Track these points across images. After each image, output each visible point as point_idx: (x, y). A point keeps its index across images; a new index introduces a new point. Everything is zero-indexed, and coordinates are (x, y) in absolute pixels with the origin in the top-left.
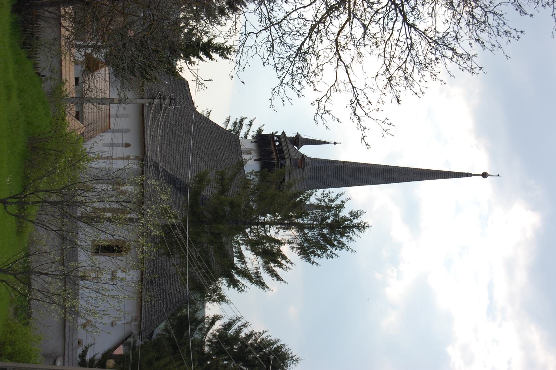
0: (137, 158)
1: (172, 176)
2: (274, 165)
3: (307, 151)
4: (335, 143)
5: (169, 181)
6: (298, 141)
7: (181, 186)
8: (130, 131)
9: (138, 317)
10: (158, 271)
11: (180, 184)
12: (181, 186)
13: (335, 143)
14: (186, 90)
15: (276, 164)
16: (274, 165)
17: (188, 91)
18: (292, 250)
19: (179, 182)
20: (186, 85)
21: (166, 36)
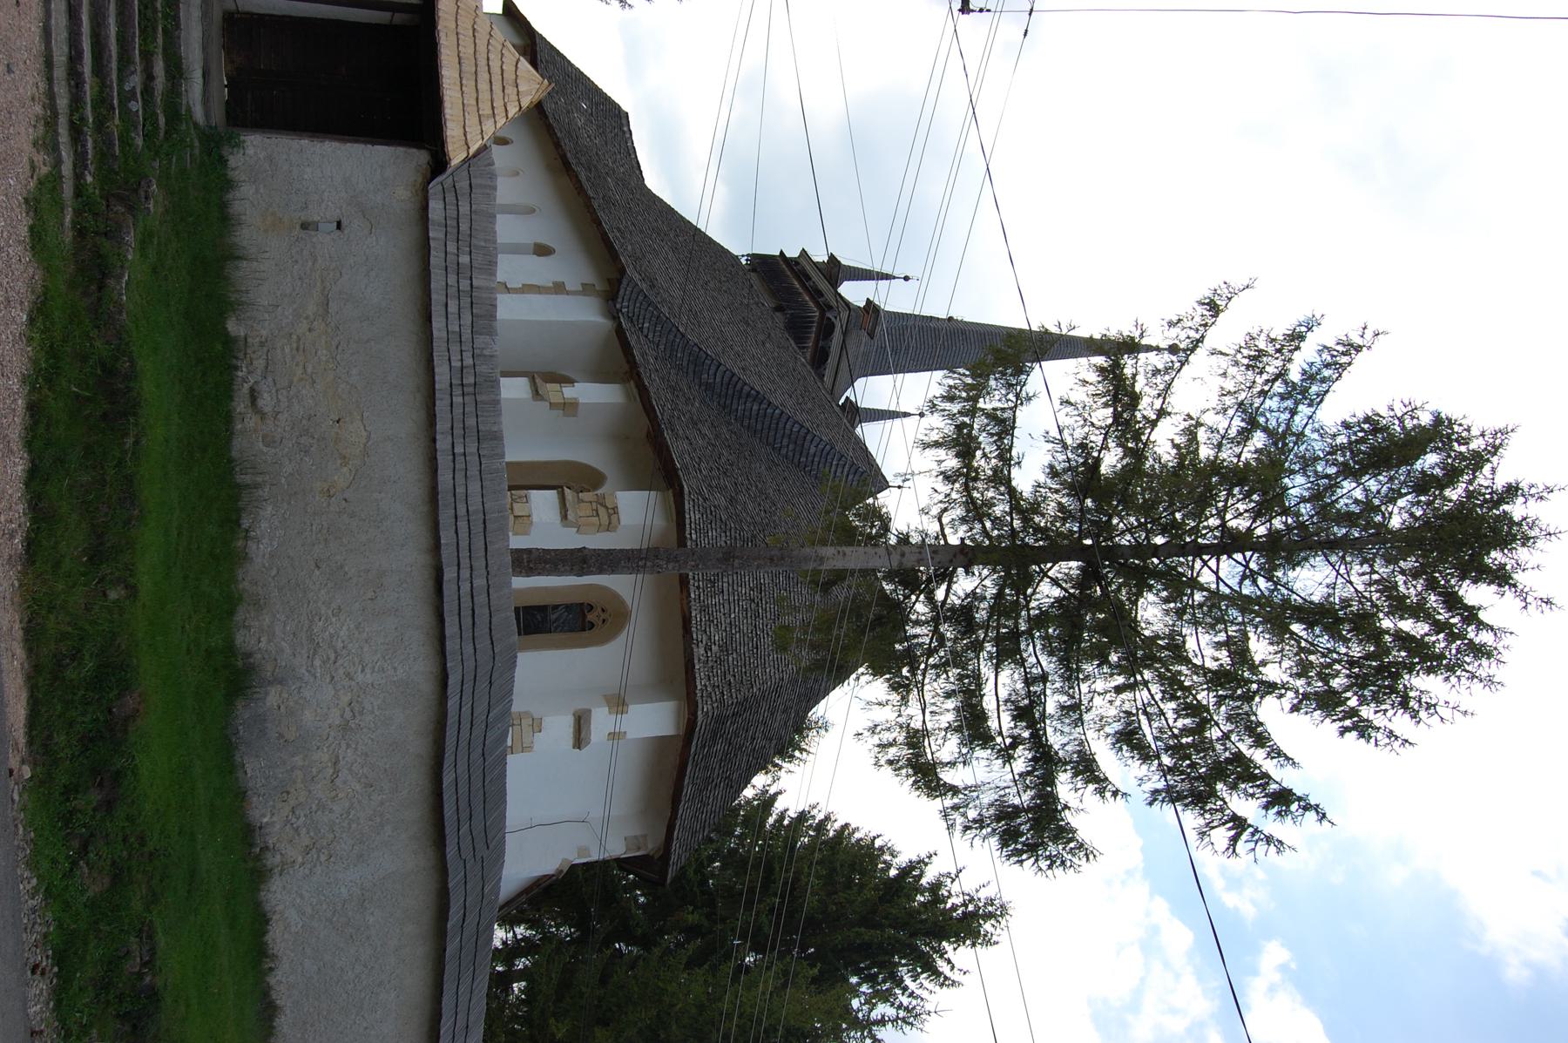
0: (586, 289)
1: (696, 349)
2: (813, 322)
3: (854, 293)
4: (906, 278)
5: (685, 364)
6: (835, 271)
7: (718, 380)
8: (534, 210)
9: (645, 836)
10: (734, 696)
11: (715, 375)
12: (718, 380)
13: (906, 278)
14: (624, 132)
15: (816, 319)
16: (813, 322)
17: (628, 135)
18: (1499, 687)
19: (713, 368)
20: (624, 122)
21: (263, 339)
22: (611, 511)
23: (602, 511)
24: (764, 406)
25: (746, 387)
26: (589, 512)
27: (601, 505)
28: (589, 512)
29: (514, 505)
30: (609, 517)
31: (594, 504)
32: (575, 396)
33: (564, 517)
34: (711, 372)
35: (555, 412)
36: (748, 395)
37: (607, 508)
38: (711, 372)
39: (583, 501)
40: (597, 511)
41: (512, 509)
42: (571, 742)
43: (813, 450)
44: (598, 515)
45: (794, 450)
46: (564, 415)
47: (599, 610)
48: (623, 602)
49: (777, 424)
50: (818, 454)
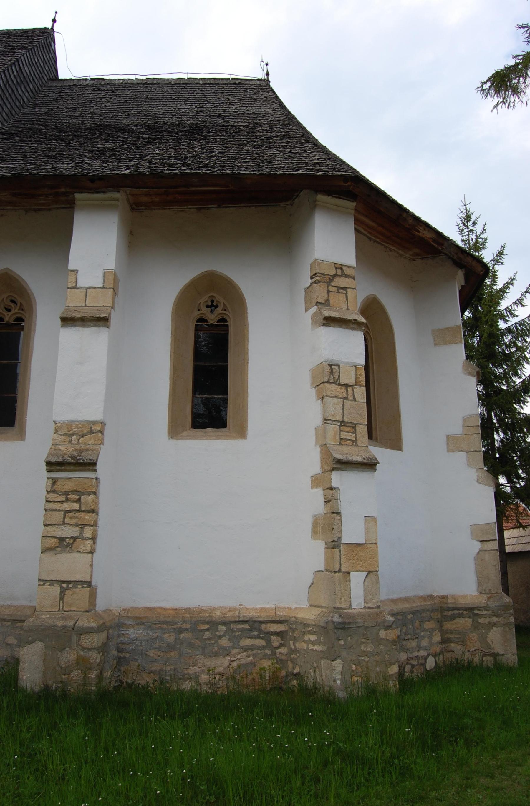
26: (342, 297)
28: (342, 297)
30: (346, 276)
41: (347, 386)
44: (345, 288)
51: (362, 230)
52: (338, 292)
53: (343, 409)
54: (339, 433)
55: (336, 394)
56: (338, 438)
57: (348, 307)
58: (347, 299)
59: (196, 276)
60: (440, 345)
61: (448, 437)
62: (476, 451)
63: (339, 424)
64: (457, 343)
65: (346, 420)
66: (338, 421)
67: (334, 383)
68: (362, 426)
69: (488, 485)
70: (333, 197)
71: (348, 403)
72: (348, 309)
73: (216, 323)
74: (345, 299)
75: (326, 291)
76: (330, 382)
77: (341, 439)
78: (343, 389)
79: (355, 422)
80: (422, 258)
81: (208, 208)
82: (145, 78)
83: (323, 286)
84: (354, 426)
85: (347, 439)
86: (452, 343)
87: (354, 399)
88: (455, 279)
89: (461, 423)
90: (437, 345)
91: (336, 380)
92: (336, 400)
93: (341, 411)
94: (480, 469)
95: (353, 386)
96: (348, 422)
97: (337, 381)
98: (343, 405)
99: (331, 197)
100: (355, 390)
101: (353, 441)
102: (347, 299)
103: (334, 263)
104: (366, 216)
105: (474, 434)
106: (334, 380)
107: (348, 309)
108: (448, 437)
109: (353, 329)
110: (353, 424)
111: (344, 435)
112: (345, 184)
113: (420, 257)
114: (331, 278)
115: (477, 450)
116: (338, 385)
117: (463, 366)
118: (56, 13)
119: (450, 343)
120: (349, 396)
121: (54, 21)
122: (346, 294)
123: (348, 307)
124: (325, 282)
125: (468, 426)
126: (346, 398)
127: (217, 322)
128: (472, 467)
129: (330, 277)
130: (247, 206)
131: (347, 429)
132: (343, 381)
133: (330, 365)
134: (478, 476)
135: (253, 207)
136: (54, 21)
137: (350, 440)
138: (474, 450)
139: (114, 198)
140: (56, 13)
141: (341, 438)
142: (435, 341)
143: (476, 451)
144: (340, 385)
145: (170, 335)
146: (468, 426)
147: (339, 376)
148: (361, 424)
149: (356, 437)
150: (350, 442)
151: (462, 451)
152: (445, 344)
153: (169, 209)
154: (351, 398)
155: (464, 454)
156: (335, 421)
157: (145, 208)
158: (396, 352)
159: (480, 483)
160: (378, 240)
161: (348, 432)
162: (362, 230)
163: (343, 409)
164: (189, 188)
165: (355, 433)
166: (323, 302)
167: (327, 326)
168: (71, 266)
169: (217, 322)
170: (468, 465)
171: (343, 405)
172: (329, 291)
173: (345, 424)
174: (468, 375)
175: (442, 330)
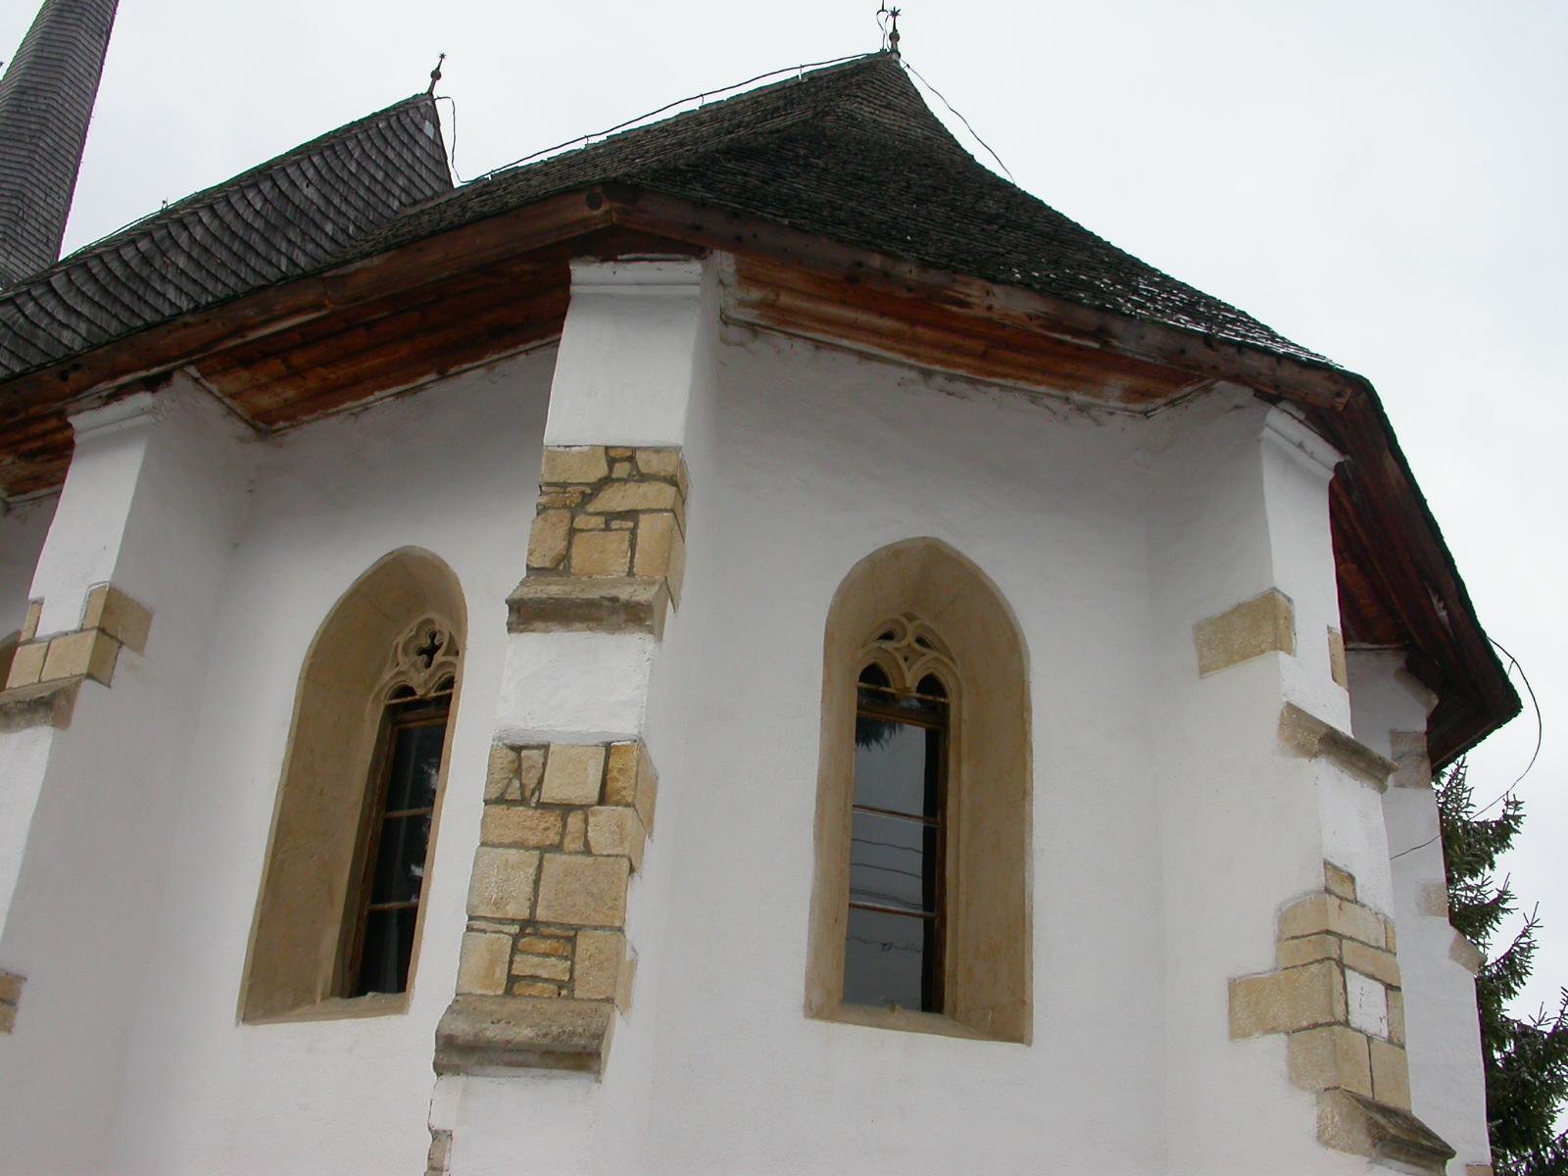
7: (84, 309)
22: (622, 470)
23: (615, 499)
24: (183, 239)
25: (128, 253)
26: (616, 542)
27: (587, 498)
28: (616, 542)
29: (548, 794)
30: (644, 478)
31: (581, 522)
32: (84, 592)
33: (635, 616)
34: (61, 316)
35: (121, 673)
36: (146, 260)
37: (606, 481)
38: (61, 316)
39: (565, 557)
40: (610, 516)
41: (566, 809)
42: (562, 1091)
43: (310, 192)
44: (632, 515)
45: (304, 234)
46: (139, 648)
47: (887, 645)
48: (895, 553)
49: (234, 234)
50: (326, 190)
51: (875, 350)
52: (607, 528)
53: (537, 882)
54: (508, 958)
55: (518, 835)
56: (501, 975)
57: (631, 567)
58: (633, 546)
59: (366, 572)
60: (1218, 668)
61: (1234, 986)
62: (1315, 1026)
63: (515, 929)
64: (1262, 652)
65: (542, 914)
66: (513, 921)
67: (523, 801)
68: (599, 933)
69: (1351, 1149)
70: (616, 260)
71: (555, 863)
72: (630, 573)
73: (433, 694)
74: (625, 546)
75: (561, 531)
76: (507, 800)
77: (512, 979)
78: (552, 819)
79: (575, 921)
80: (1172, 403)
81: (421, 388)
82: (604, 137)
83: (554, 519)
84: (572, 933)
85: (535, 978)
86: (1249, 657)
87: (587, 850)
88: (1259, 441)
89: (1269, 929)
90: (1206, 671)
91: (528, 793)
92: (513, 855)
93: (528, 889)
94: (1327, 1089)
95: (588, 806)
96: (547, 924)
97: (533, 794)
98: (540, 868)
99: (612, 263)
100: (591, 820)
101: (561, 985)
102: (633, 546)
103: (607, 448)
104: (843, 303)
105: (1311, 963)
106: (522, 794)
107: (630, 573)
108: (1234, 986)
109: (614, 629)
110: (570, 927)
111: (524, 965)
112: (595, 213)
113: (1160, 401)
114: (588, 491)
115: (1321, 1021)
116: (536, 808)
117: (1281, 725)
118: (442, 56)
119: (1245, 656)
120: (567, 841)
121: (436, 75)
122: (633, 532)
123: (631, 567)
124: (565, 506)
125: (1293, 938)
126: (558, 848)
127: (435, 691)
128: (1303, 1088)
129: (583, 488)
130: (507, 357)
131: (543, 946)
132: (551, 792)
133: (517, 749)
134: (1320, 1118)
135: (523, 357)
136: (436, 75)
137: (546, 980)
138: (1312, 1022)
139: (142, 409)
140: (442, 56)
141: (514, 972)
142: (1201, 659)
143: (1315, 1026)
144: (542, 806)
145: (286, 739)
146: (1293, 938)
147: (541, 781)
148: (596, 928)
149: (571, 971)
150: (546, 985)
151: (1274, 1030)
152: (1230, 661)
153: (339, 412)
154: (572, 843)
155: (1279, 1040)
156: (500, 921)
157: (287, 424)
158: (1029, 710)
159: (1327, 1143)
160: (961, 372)
161: (547, 955)
162: (875, 350)
163: (537, 882)
164: (244, 336)
165: (571, 957)
166: (547, 565)
167: (521, 631)
168: (33, 594)
169: (435, 691)
170: (1290, 1079)
171: (540, 868)
172: (572, 532)
173: (536, 930)
174: (1296, 756)
175: (1224, 616)
